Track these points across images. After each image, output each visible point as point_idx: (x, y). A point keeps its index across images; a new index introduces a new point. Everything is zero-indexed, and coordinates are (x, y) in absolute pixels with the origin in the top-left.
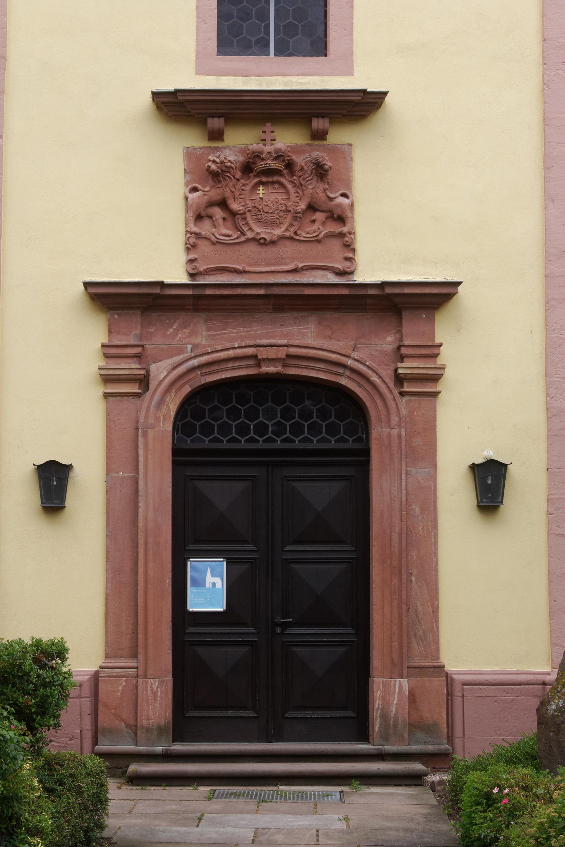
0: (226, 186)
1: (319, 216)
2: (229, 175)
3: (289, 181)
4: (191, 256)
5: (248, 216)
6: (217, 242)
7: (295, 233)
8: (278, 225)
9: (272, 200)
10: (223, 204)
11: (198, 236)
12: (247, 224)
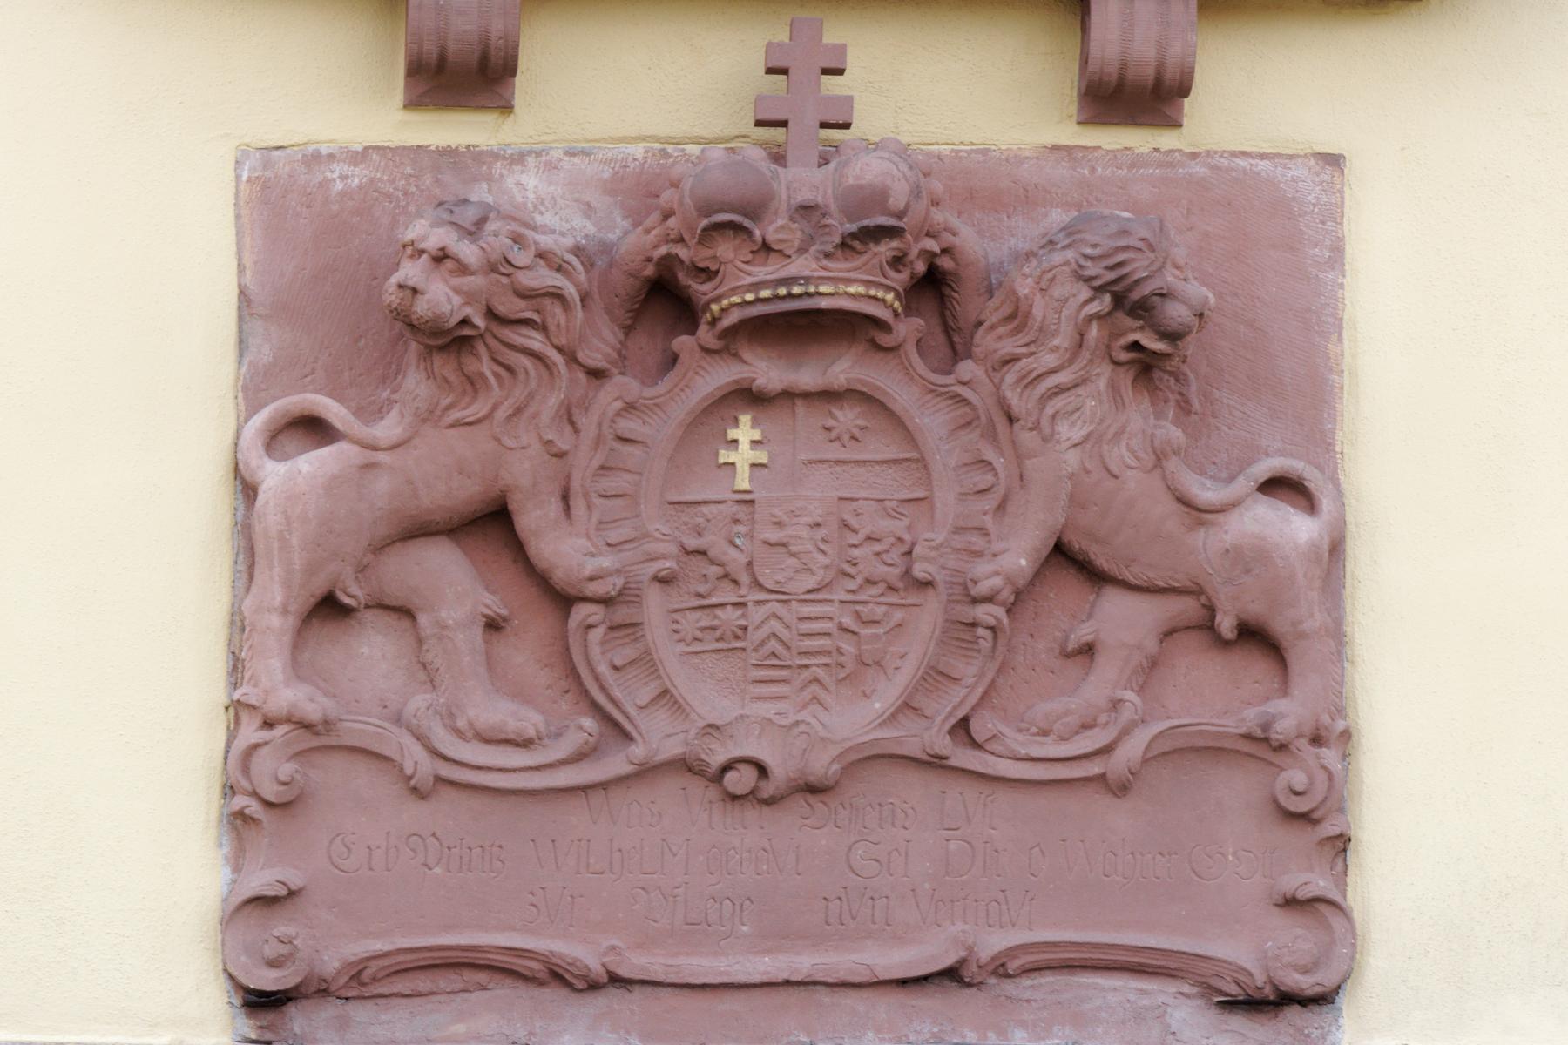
1: (1123, 620)
2: (535, 341)
3: (932, 390)
4: (261, 881)
5: (655, 605)
6: (440, 780)
7: (962, 728)
8: (862, 671)
10: (491, 523)
11: (315, 736)
12: (647, 662)
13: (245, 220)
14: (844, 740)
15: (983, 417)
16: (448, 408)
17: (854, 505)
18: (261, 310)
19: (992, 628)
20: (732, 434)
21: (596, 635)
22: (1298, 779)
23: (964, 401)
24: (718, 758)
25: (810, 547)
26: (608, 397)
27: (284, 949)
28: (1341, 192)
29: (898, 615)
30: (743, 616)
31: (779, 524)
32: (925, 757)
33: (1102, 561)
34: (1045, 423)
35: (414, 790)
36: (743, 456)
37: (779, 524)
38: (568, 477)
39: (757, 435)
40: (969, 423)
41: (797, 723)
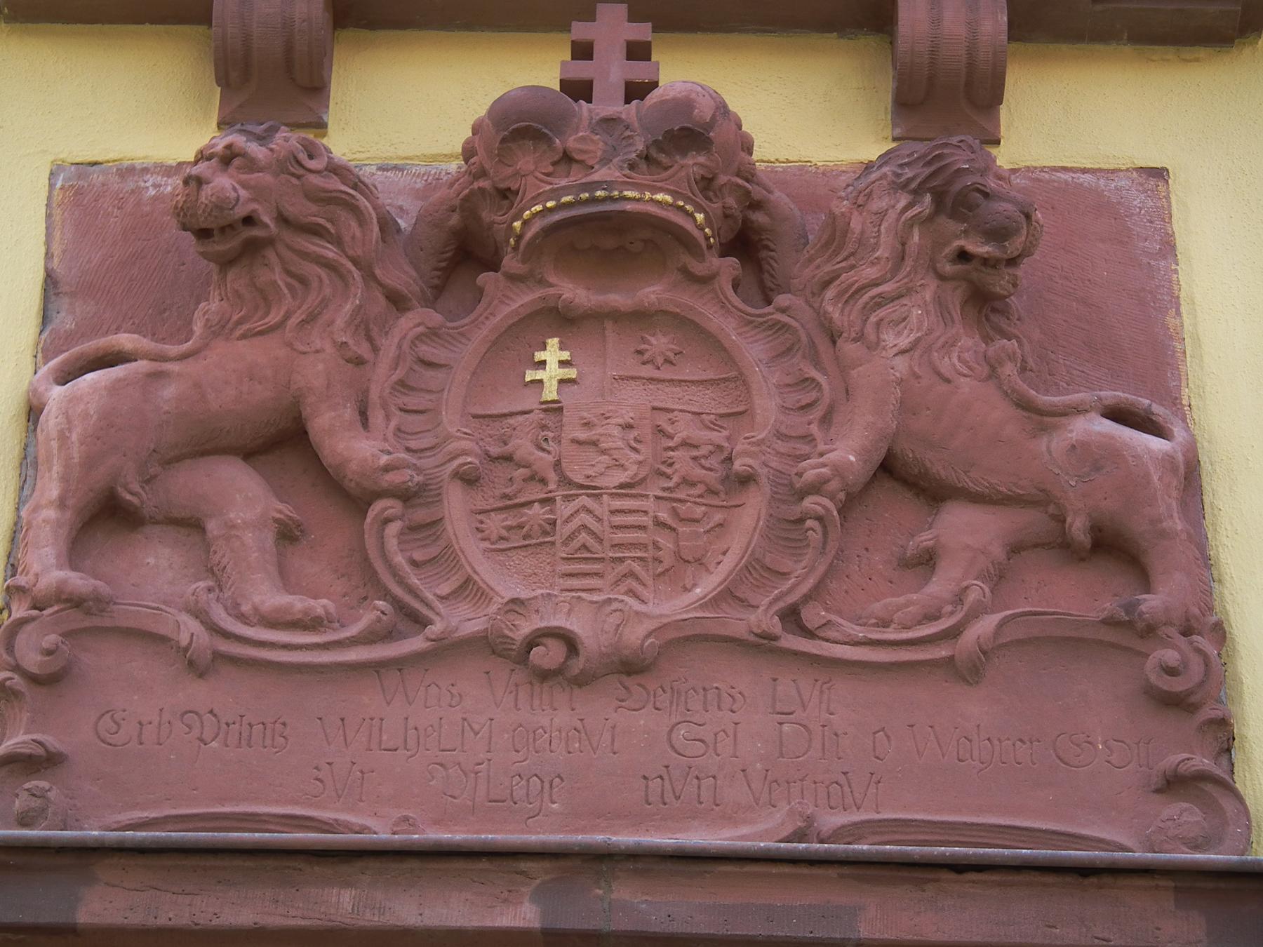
0: (311, 319)
1: (966, 530)
2: (330, 252)
5: (456, 506)
6: (218, 656)
9: (628, 416)
10: (281, 441)
12: (448, 559)
13: (57, 218)
14: (661, 616)
15: (804, 338)
16: (240, 322)
17: (670, 416)
18: (66, 289)
19: (819, 519)
20: (540, 356)
21: (393, 528)
22: (1170, 656)
23: (785, 326)
24: (526, 628)
25: (620, 444)
26: (410, 323)
27: (36, 803)
28: (1168, 198)
29: (718, 517)
30: (551, 512)
31: (588, 425)
32: (752, 638)
33: (939, 467)
34: (869, 329)
35: (191, 663)
36: (551, 374)
37: (588, 425)
38: (366, 391)
39: (565, 355)
40: (789, 349)
41: (609, 601)
